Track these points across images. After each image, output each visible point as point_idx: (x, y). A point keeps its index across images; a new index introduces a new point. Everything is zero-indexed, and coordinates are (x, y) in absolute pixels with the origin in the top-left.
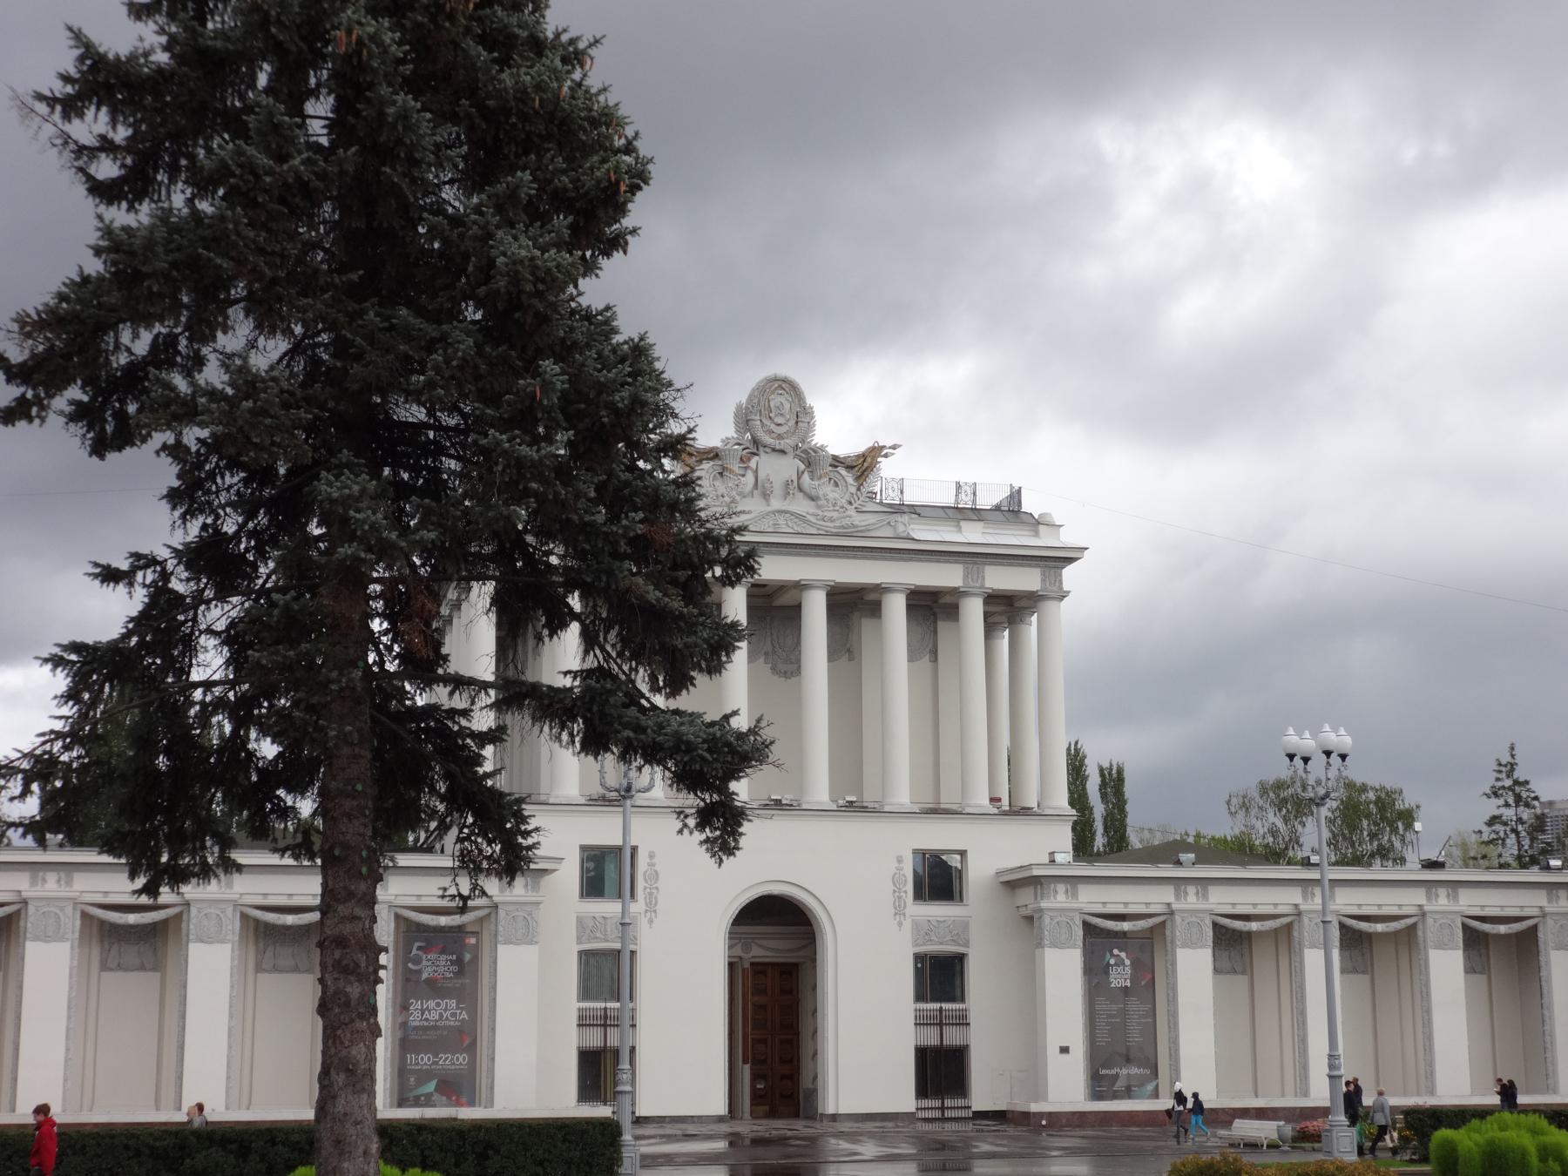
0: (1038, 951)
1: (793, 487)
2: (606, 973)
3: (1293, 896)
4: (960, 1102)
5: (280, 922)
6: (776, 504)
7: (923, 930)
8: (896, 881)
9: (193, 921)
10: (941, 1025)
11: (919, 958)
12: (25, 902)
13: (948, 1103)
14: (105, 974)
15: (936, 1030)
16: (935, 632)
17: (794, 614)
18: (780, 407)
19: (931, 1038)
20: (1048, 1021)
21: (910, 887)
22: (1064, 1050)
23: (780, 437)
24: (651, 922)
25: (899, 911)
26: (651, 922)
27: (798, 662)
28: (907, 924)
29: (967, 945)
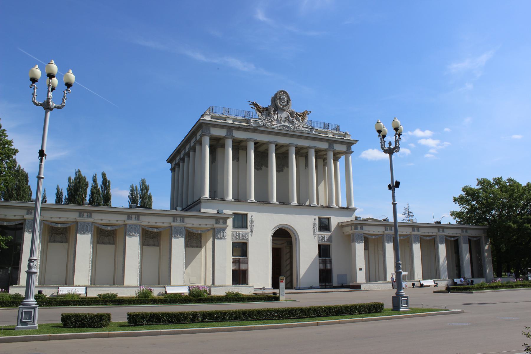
0: (352, 244)
1: (287, 119)
2: (241, 249)
3: (75, 215)
4: (330, 284)
5: (56, 226)
6: (283, 124)
7: (321, 239)
8: (314, 224)
9: (27, 225)
10: (325, 263)
11: (320, 246)
12: (25, 220)
13: (327, 284)
14: (98, 245)
15: (324, 264)
16: (239, 153)
17: (245, 149)
18: (283, 98)
19: (323, 267)
20: (301, 261)
21: (317, 227)
22: (361, 269)
23: (283, 106)
24: (251, 235)
25: (315, 234)
26: (251, 235)
27: (268, 164)
28: (317, 236)
29: (331, 242)
